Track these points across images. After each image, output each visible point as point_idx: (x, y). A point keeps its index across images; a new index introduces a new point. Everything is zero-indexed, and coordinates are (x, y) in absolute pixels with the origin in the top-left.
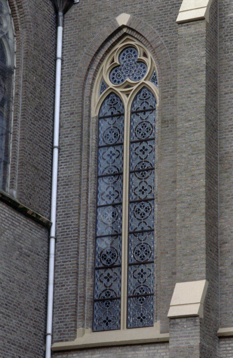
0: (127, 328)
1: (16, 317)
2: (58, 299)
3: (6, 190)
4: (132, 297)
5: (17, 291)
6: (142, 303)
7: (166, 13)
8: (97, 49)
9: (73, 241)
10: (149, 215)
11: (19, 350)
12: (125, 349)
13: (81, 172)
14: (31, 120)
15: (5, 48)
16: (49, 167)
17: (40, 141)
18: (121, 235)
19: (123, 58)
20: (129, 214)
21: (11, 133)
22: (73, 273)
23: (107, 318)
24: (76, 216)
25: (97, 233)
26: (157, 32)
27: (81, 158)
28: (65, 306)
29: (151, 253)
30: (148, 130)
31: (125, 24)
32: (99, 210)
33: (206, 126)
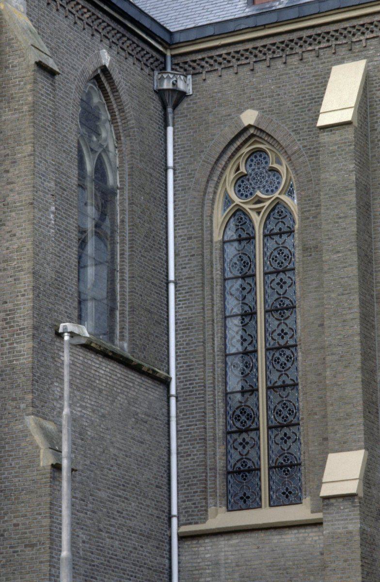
0: (270, 506)
1: (135, 499)
2: (183, 472)
3: (116, 343)
4: (275, 467)
5: (135, 468)
6: (286, 474)
7: (304, 110)
8: (218, 155)
9: (199, 392)
10: (292, 365)
11: (141, 539)
12: (268, 533)
13: (204, 312)
14: (140, 252)
15: (105, 164)
16: (165, 308)
17: (153, 276)
18: (257, 390)
19: (251, 166)
20: (266, 364)
21: (117, 271)
22: (200, 439)
23: (245, 494)
24: (201, 368)
25: (228, 389)
26: (292, 134)
27: (203, 294)
28: (192, 481)
29: (296, 413)
30: (286, 257)
31: (252, 123)
32: (228, 283)
33: (359, 258)
